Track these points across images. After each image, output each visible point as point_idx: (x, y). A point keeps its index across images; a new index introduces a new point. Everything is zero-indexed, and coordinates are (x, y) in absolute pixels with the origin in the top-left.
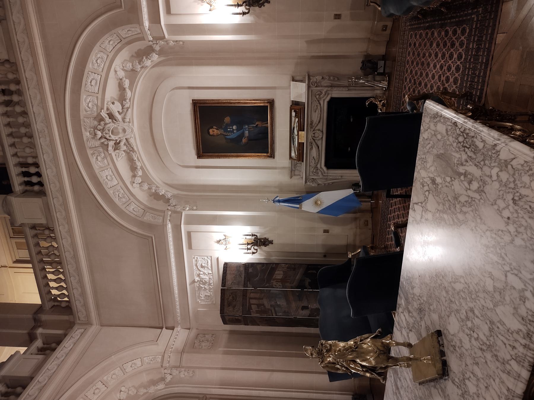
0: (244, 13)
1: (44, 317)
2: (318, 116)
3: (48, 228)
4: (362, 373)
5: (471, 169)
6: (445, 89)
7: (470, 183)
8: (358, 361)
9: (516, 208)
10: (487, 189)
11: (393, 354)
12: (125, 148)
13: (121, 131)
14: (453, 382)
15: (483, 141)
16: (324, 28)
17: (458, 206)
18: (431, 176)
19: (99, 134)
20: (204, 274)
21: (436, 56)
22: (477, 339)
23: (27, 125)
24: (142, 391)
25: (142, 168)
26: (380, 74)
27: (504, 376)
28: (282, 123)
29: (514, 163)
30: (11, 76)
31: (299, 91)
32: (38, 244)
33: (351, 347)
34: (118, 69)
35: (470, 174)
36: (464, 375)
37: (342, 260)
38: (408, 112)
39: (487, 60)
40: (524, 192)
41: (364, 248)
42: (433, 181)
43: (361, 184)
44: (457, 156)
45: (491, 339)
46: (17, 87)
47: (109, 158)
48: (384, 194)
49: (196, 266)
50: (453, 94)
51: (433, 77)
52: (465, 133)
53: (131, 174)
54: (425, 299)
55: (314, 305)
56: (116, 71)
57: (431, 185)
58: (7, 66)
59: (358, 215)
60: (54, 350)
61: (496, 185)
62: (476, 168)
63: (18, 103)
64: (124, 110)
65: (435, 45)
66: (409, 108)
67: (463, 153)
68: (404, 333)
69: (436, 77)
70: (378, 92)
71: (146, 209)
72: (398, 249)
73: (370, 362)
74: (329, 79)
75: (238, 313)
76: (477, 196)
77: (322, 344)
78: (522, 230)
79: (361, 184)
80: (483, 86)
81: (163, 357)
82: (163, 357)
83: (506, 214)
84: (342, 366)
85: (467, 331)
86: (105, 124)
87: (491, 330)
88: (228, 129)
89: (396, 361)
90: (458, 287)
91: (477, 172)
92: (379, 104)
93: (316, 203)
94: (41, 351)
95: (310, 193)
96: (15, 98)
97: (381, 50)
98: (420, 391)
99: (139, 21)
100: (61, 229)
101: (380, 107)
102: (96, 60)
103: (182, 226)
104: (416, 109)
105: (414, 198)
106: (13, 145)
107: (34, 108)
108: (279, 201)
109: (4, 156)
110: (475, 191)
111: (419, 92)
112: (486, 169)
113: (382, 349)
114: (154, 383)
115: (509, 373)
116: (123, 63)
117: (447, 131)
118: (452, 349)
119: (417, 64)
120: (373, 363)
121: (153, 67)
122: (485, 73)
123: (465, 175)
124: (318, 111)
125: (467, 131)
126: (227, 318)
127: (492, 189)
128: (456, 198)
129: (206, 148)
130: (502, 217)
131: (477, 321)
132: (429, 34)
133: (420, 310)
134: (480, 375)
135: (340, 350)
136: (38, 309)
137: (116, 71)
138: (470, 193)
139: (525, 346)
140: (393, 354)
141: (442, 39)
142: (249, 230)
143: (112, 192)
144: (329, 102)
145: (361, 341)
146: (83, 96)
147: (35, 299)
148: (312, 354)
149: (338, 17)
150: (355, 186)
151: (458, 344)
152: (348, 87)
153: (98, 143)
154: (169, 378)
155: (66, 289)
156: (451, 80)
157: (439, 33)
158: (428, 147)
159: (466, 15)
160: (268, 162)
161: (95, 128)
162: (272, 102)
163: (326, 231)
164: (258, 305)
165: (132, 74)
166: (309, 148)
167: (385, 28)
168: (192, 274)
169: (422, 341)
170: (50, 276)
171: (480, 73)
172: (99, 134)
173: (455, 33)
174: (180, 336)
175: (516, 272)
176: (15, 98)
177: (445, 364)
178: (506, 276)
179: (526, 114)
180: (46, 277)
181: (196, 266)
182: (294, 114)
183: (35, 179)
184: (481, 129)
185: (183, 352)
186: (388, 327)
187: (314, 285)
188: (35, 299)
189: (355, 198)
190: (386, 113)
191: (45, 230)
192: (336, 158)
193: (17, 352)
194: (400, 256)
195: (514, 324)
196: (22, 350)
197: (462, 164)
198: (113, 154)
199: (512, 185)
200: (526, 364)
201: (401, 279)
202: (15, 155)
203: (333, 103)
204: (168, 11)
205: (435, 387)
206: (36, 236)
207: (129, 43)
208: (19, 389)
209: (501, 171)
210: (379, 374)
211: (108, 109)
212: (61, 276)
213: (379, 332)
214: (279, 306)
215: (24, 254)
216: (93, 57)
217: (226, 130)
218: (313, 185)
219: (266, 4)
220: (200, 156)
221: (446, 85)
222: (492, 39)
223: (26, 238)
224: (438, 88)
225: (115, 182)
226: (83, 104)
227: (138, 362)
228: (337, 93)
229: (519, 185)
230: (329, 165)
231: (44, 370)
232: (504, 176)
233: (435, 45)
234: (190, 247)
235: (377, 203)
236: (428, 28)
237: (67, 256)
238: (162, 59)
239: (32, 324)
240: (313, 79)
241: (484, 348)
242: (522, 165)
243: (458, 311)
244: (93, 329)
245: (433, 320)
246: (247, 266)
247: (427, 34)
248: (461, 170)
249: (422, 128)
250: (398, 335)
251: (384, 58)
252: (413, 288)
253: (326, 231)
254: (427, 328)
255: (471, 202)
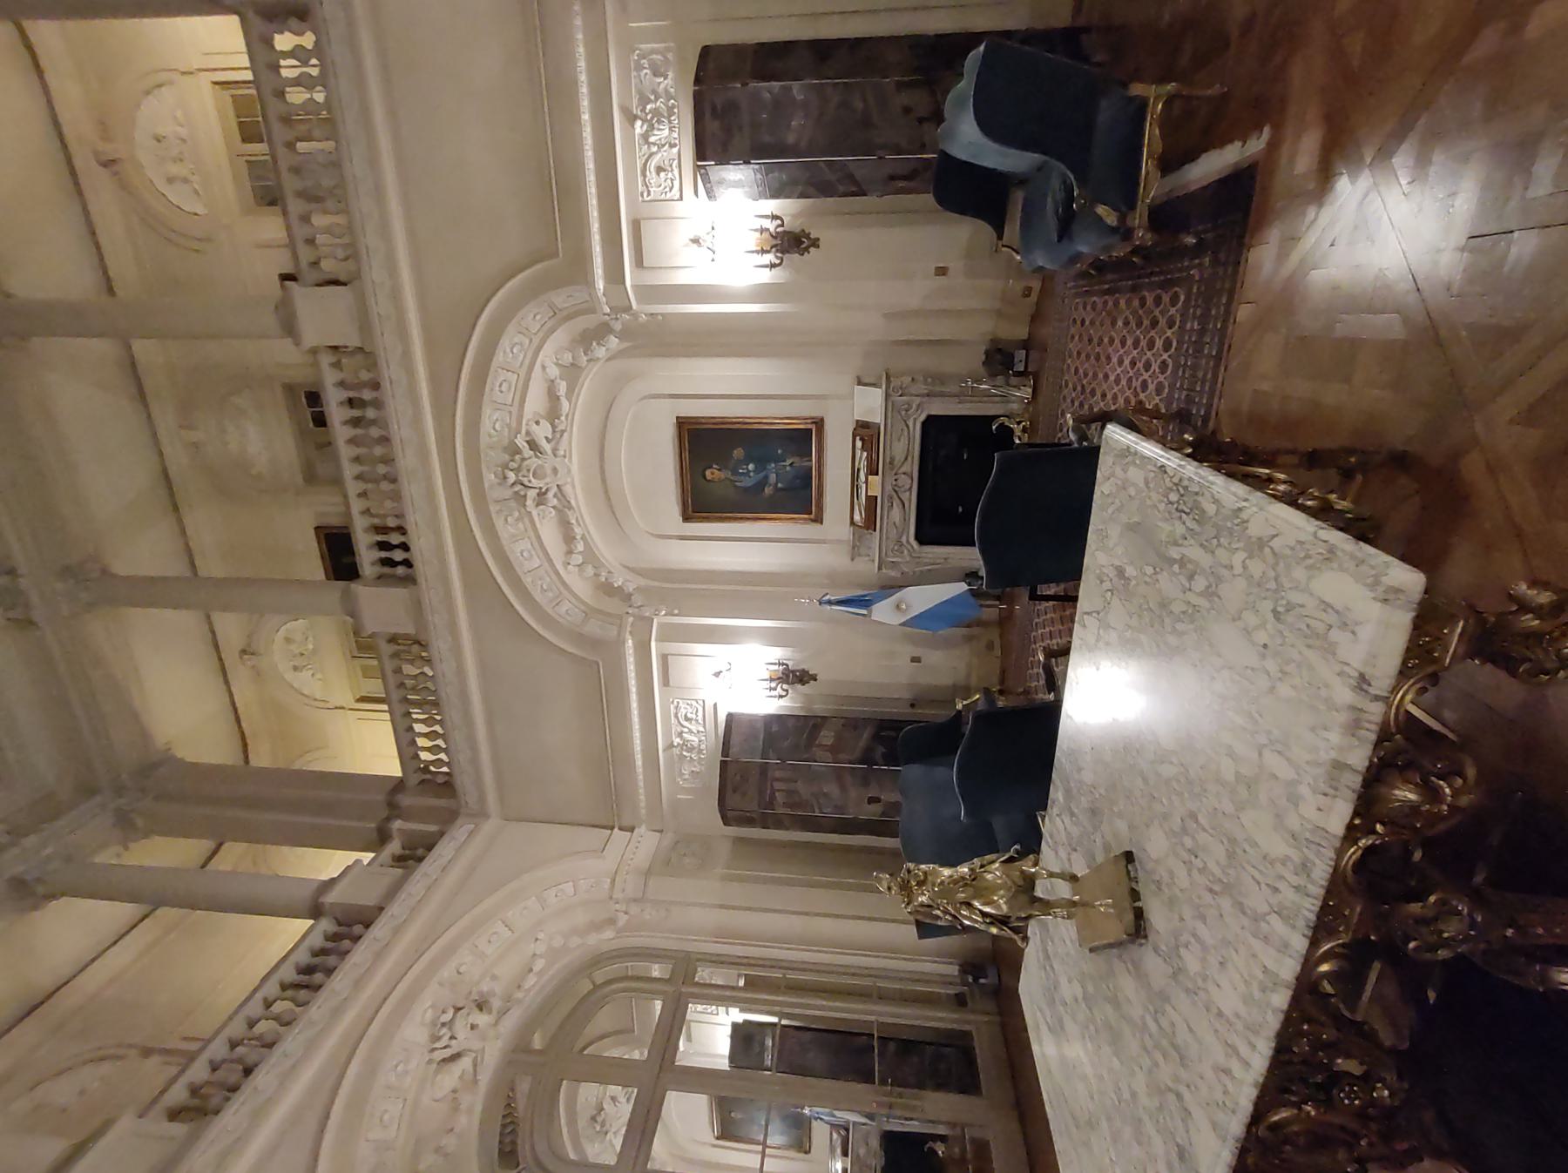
0: (773, 266)
1: (405, 800)
2: (905, 448)
3: (418, 643)
4: (982, 927)
5: (1194, 552)
6: (1141, 402)
7: (1191, 578)
8: (976, 904)
9: (1280, 627)
10: (1224, 590)
11: (1039, 893)
12: (555, 502)
13: (549, 471)
14: (1156, 950)
15: (1216, 501)
16: (916, 292)
17: (1167, 620)
18: (1117, 563)
19: (512, 477)
20: (691, 732)
21: (1123, 343)
22: (1203, 871)
23: (388, 460)
24: (575, 941)
25: (583, 538)
26: (1019, 374)
27: (1257, 945)
28: (837, 461)
29: (1276, 543)
30: (365, 376)
31: (870, 404)
32: (398, 671)
33: (963, 878)
34: (548, 363)
35: (1190, 561)
36: (1176, 939)
37: (941, 715)
38: (1070, 444)
39: (1220, 352)
40: (1296, 597)
41: (987, 692)
42: (1120, 572)
43: (983, 573)
44: (1169, 528)
45: (1231, 871)
46: (375, 394)
47: (526, 520)
48: (1024, 593)
49: (676, 716)
50: (1155, 414)
51: (1118, 381)
52: (1180, 486)
53: (564, 548)
54: (1102, 791)
55: (890, 796)
56: (544, 368)
57: (1115, 580)
58: (359, 357)
59: (975, 630)
60: (420, 860)
61: (1241, 584)
62: (1202, 551)
63: (373, 422)
64: (556, 436)
65: (1120, 323)
66: (1072, 437)
67: (1177, 523)
68: (1063, 854)
69: (1124, 382)
70: (1015, 406)
71: (590, 612)
72: (1052, 696)
73: (999, 907)
74: (925, 382)
75: (752, 805)
76: (1203, 602)
77: (909, 871)
78: (1290, 668)
79: (983, 573)
80: (1211, 397)
81: (613, 881)
82: (613, 881)
83: (1262, 637)
84: (946, 912)
85: (1185, 855)
86: (523, 459)
87: (1231, 855)
88: (737, 469)
89: (1046, 906)
90: (1168, 771)
91: (1204, 559)
92: (1018, 430)
93: (898, 607)
94: (399, 860)
95: (889, 588)
96: (370, 413)
97: (1021, 332)
98: (1090, 964)
99: (587, 280)
100: (440, 645)
101: (1018, 433)
102: (511, 348)
103: (653, 644)
104: (1086, 439)
105: (1083, 604)
106: (363, 495)
107: (401, 431)
108: (830, 602)
109: (348, 514)
110: (1201, 594)
111: (1091, 408)
112: (1220, 552)
113: (1021, 883)
114: (596, 927)
115: (1266, 939)
116: (556, 353)
117: (1147, 483)
118: (1153, 887)
119: (1088, 357)
120: (1005, 907)
121: (609, 359)
122: (1215, 376)
123: (1182, 562)
124: (904, 441)
125: (1186, 483)
126: (730, 814)
127: (1234, 591)
128: (1164, 605)
129: (699, 504)
130: (1254, 644)
131: (1203, 838)
132: (1110, 303)
133: (1094, 812)
134: (1210, 941)
135: (942, 882)
136: (398, 786)
137: (544, 368)
138: (1191, 597)
139: (1297, 888)
140: (1039, 893)
141: (1134, 313)
142: (777, 653)
143: (529, 580)
144: (924, 424)
145: (982, 866)
146: (487, 411)
147: (397, 772)
148: (889, 889)
149: (942, 271)
150: (971, 576)
151: (1166, 879)
152: (960, 396)
153: (508, 493)
154: (623, 919)
155: (445, 751)
156: (1152, 387)
157: (1128, 302)
158: (1110, 511)
159: (1180, 270)
160: (811, 530)
161: (506, 467)
162: (819, 423)
163: (916, 660)
164: (790, 793)
165: (572, 373)
166: (886, 504)
167: (1027, 292)
168: (667, 733)
169: (1096, 870)
170: (418, 728)
171: (1205, 375)
172: (512, 477)
173: (1158, 301)
174: (645, 844)
175: (1279, 747)
176: (370, 413)
177: (1139, 914)
178: (1260, 754)
179: (1292, 452)
180: (411, 729)
181: (676, 716)
182: (859, 444)
183: (398, 555)
184: (1211, 478)
185: (648, 873)
186: (1031, 842)
187: (891, 759)
188: (397, 772)
189: (972, 600)
190: (1030, 445)
191: (411, 646)
192: (938, 523)
193: (358, 861)
194: (1052, 712)
195: (1279, 847)
196: (367, 857)
197: (1176, 544)
198: (534, 513)
199: (1272, 585)
200: (1301, 923)
201: (1057, 754)
202: (367, 512)
203: (931, 423)
204: (639, 262)
205: (1120, 957)
206: (396, 655)
207: (569, 318)
208: (357, 929)
209: (1250, 557)
210: (1016, 930)
211: (528, 433)
212: (437, 728)
213: (1017, 852)
214: (825, 795)
215: (375, 687)
216: (505, 342)
217: (735, 472)
218: (893, 573)
219: (812, 249)
220: (687, 518)
221: (1142, 396)
222: (1228, 313)
223: (379, 658)
224: (1127, 401)
225: (536, 562)
226: (486, 425)
227: (568, 888)
228: (940, 408)
229: (1287, 585)
230: (923, 538)
231: (402, 896)
232: (1256, 568)
233: (1120, 323)
234: (666, 682)
235: (1011, 611)
236: (1109, 292)
237: (448, 693)
238: (626, 345)
239: (385, 813)
240: (895, 382)
241: (1217, 888)
242: (1292, 549)
243: (1166, 817)
244: (488, 827)
245: (1118, 833)
246: (779, 718)
247: (1106, 302)
248: (1174, 553)
249: (1099, 474)
250: (1051, 857)
251: (1026, 345)
252: (1080, 770)
253: (916, 660)
254: (1107, 848)
255: (1192, 613)
